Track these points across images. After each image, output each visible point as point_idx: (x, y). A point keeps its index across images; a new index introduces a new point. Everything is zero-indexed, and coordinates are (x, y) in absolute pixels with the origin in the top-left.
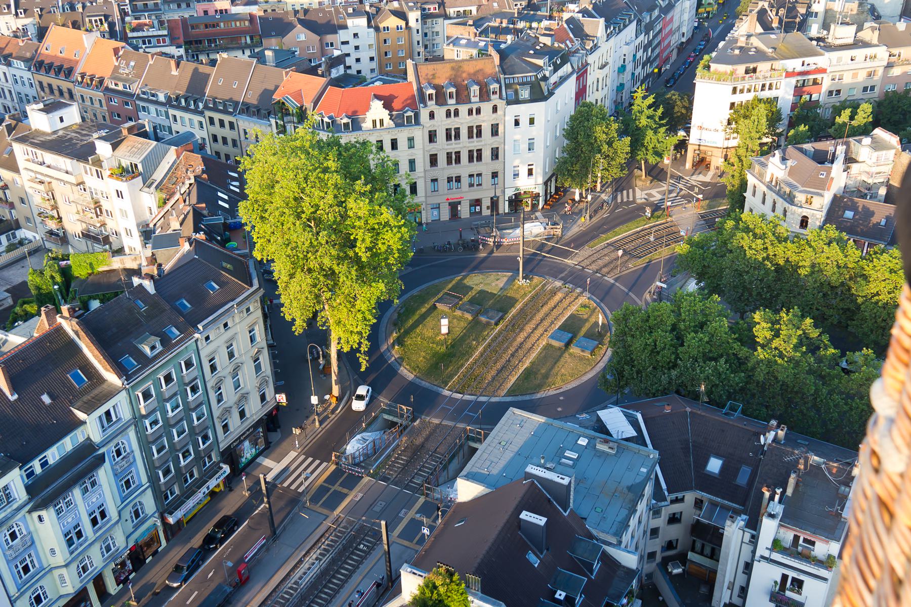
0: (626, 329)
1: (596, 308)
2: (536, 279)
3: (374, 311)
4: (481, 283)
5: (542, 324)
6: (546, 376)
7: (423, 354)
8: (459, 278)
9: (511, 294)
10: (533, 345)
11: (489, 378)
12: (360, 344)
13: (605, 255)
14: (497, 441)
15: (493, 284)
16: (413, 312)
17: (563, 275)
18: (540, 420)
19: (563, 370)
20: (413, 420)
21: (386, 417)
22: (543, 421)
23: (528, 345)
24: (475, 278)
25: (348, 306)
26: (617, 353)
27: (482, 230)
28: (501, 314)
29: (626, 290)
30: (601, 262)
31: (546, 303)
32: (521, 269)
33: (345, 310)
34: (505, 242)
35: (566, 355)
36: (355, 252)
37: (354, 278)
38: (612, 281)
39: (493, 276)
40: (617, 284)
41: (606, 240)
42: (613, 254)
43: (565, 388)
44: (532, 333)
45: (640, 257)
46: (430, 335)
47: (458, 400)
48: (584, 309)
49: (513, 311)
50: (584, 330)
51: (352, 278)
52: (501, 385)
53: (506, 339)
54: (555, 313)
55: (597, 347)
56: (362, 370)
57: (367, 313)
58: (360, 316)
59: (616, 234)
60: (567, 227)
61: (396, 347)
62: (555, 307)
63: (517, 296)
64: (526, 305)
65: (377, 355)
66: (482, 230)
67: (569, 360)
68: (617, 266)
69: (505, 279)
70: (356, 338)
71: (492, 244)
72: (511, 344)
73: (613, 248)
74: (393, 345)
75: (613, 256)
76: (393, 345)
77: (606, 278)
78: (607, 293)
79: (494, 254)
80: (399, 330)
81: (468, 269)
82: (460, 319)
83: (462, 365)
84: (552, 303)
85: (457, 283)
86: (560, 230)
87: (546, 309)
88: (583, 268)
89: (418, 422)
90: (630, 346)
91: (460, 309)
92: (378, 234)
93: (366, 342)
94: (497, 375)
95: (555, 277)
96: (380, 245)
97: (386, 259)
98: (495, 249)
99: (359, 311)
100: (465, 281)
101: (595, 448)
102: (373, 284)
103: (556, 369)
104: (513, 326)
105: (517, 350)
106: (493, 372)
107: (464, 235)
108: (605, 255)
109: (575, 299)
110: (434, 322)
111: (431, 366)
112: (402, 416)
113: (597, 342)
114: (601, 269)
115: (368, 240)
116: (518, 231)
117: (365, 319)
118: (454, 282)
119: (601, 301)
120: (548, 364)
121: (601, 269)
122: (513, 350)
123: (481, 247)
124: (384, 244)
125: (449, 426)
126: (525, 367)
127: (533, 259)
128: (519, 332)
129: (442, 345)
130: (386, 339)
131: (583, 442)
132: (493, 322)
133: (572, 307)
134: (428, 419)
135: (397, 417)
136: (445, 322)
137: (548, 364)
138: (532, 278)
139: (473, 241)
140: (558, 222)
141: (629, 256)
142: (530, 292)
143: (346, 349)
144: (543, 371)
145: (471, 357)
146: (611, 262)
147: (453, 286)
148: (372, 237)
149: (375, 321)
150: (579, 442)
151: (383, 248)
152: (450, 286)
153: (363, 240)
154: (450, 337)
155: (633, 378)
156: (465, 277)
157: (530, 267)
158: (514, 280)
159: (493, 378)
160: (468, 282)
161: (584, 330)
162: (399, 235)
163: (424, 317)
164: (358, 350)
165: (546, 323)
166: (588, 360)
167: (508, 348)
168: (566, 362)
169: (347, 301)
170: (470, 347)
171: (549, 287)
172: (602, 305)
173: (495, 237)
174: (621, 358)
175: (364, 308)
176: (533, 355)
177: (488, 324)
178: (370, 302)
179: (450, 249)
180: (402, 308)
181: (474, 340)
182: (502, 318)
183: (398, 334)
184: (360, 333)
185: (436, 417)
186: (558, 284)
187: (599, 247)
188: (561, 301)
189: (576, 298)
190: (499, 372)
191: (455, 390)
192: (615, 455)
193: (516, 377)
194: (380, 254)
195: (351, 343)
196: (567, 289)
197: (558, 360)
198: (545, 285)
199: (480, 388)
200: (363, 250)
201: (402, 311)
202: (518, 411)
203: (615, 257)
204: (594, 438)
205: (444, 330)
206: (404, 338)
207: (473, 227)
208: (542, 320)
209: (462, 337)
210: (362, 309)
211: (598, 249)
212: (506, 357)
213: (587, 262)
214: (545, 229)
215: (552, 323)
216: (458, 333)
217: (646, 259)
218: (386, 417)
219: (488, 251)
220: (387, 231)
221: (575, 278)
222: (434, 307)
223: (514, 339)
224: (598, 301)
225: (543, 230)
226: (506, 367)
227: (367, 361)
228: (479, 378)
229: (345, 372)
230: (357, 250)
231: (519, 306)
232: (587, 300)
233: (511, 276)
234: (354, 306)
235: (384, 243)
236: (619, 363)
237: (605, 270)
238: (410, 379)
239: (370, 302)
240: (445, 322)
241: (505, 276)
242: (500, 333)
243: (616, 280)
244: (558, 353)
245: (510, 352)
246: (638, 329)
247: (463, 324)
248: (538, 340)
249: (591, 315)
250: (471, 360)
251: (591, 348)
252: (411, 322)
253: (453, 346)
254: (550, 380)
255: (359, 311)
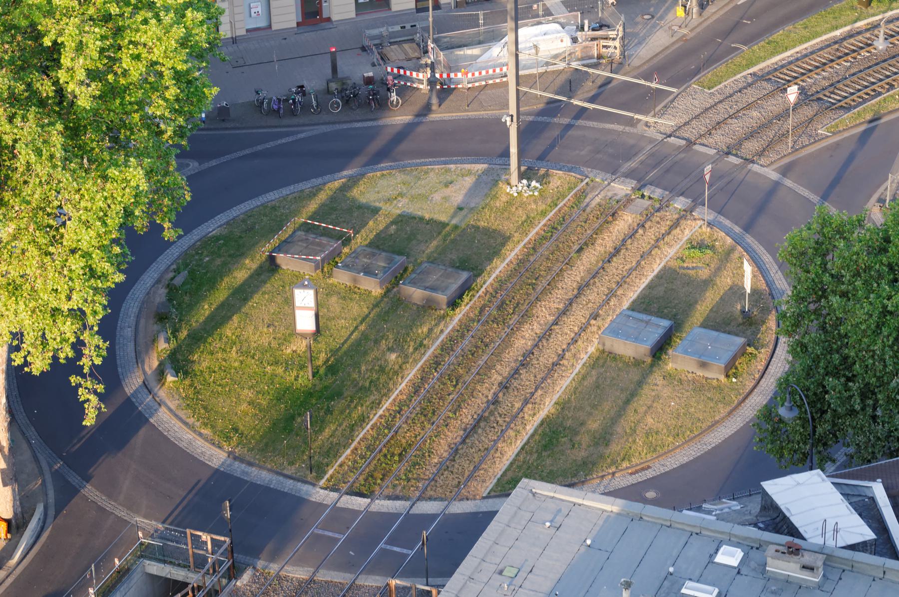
0: (826, 278)
1: (731, 250)
2: (559, 179)
3: (117, 250)
4: (401, 195)
5: (583, 299)
6: (603, 438)
7: (248, 394)
8: (337, 184)
9: (487, 220)
10: (562, 357)
11: (442, 449)
12: (78, 346)
13: (749, 107)
14: (493, 568)
15: (437, 197)
16: (212, 283)
17: (632, 164)
18: (608, 508)
19: (650, 420)
20: (234, 572)
21: (155, 568)
22: (615, 509)
23: (547, 356)
24: (384, 182)
25: (42, 241)
26: (804, 346)
27: (394, 52)
28: (465, 275)
29: (814, 198)
30: (737, 127)
31: (589, 242)
32: (514, 150)
33: (33, 251)
34: (462, 79)
35: (657, 378)
36: (56, 83)
37: (59, 154)
38: (774, 176)
39: (434, 173)
40: (788, 183)
41: (748, 66)
42: (772, 101)
43: (658, 468)
44: (556, 323)
45: (848, 108)
46: (265, 341)
47: (355, 513)
48: (697, 253)
49: (499, 268)
50: (702, 310)
51: (52, 157)
52: (476, 468)
53: (482, 344)
54: (618, 266)
55: (742, 352)
56: (87, 422)
57: (97, 255)
58: (76, 264)
59: (778, 48)
60: (635, 35)
61: (170, 378)
62: (617, 251)
63: (507, 227)
64: (534, 248)
65: (118, 401)
66: (394, 52)
67: (666, 392)
68: (785, 135)
69: (469, 181)
70: (68, 328)
71: (424, 87)
72: (497, 355)
73: (769, 87)
74: (160, 374)
75: (773, 106)
76: (160, 374)
77: (755, 168)
78: (761, 208)
79: (433, 117)
80: (175, 332)
81: (362, 159)
82: (348, 294)
83: (363, 420)
84: (607, 241)
85: (333, 199)
86: (617, 43)
87: (590, 258)
88: (690, 143)
89: (246, 577)
90: (840, 322)
91: (346, 267)
92: (118, 31)
93: (97, 340)
94: (463, 442)
95: (613, 171)
96: (126, 63)
97: (141, 104)
98: (435, 101)
99: (73, 251)
100: (355, 193)
101: (764, 571)
102: (113, 172)
103: (625, 424)
104: (500, 308)
105: (516, 372)
106: (453, 435)
107: (344, 68)
108: (749, 107)
109: (672, 228)
110: (273, 308)
111: (274, 424)
112: (200, 562)
113: (740, 341)
114: (740, 143)
115: (93, 46)
116: (498, 52)
117: (92, 273)
118: (322, 197)
119: (747, 228)
120: (607, 406)
121: (740, 143)
122: (506, 371)
123: (394, 97)
124: (137, 57)
125: (335, 585)
126: (542, 415)
127: (545, 126)
128: (520, 323)
129: (302, 367)
130: (139, 358)
131: (730, 556)
132: (442, 298)
133: (666, 249)
134: (274, 568)
135: (186, 567)
136: (304, 298)
137: (608, 406)
138: (546, 175)
139: (369, 81)
140: (610, 21)
141: (816, 106)
142: (543, 213)
143: (39, 365)
144: (594, 425)
145: (386, 396)
146: (764, 126)
147: (322, 206)
148: (103, 38)
149: (120, 278)
150: (720, 558)
151: (136, 71)
152: (313, 206)
153: (80, 47)
154: (322, 346)
155: (852, 412)
156: (354, 181)
157: (539, 146)
158: (495, 183)
159: (455, 452)
160: (363, 193)
161: (702, 310)
162: (179, 32)
163: (243, 294)
164: (73, 366)
165: (593, 296)
166: (719, 388)
167: (489, 367)
168: (657, 397)
169: (39, 228)
170: (382, 370)
171: (595, 200)
172: (749, 239)
173: (433, 67)
174: (816, 360)
175: (87, 239)
176: (563, 384)
177: (429, 306)
178: (105, 224)
179: (306, 107)
180: (177, 271)
181: (391, 350)
182: (466, 288)
183: (173, 344)
184: (78, 314)
185: (300, 562)
186: (622, 188)
187: (729, 84)
188: (632, 235)
189: (676, 224)
190: (471, 431)
191: (344, 487)
192: (819, 587)
193: (519, 444)
194: (126, 88)
195: (53, 345)
196: (646, 203)
197: (632, 395)
198: (583, 193)
199: (418, 479)
200: (81, 75)
201: (179, 281)
202: (544, 489)
203: (777, 110)
204: (760, 546)
205: (305, 322)
206: (191, 352)
207: (367, 43)
208: (582, 289)
209: (358, 343)
210: (84, 246)
211: (729, 91)
212: (487, 391)
213: (699, 127)
214: (574, 40)
215: (611, 294)
216: (345, 334)
217: (865, 112)
218: (155, 568)
219: (417, 108)
220: (145, 22)
221: (668, 171)
222: (271, 265)
223: (507, 343)
224: (737, 229)
225: (568, 42)
226: (486, 419)
227: (101, 397)
228: (412, 452)
229: (27, 455)
230: (62, 76)
231: (512, 253)
232: (706, 230)
233: (486, 172)
234: (55, 241)
235: (137, 57)
236: (809, 372)
237: (752, 146)
238: (215, 463)
239: (105, 224)
240: (304, 298)
241: (470, 173)
242: (464, 329)
243: (785, 171)
244: (635, 375)
245: (496, 378)
246: (857, 274)
247: (358, 309)
248: (574, 341)
249: (718, 269)
250: (386, 404)
251: (727, 356)
252: (206, 309)
253: (332, 369)
254: (614, 448)
255: (73, 251)
